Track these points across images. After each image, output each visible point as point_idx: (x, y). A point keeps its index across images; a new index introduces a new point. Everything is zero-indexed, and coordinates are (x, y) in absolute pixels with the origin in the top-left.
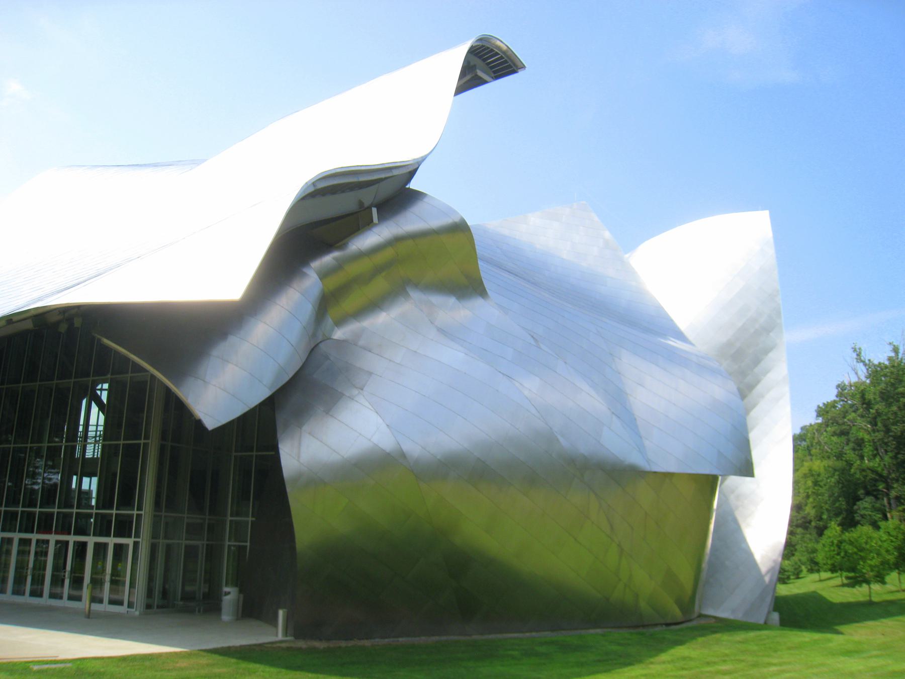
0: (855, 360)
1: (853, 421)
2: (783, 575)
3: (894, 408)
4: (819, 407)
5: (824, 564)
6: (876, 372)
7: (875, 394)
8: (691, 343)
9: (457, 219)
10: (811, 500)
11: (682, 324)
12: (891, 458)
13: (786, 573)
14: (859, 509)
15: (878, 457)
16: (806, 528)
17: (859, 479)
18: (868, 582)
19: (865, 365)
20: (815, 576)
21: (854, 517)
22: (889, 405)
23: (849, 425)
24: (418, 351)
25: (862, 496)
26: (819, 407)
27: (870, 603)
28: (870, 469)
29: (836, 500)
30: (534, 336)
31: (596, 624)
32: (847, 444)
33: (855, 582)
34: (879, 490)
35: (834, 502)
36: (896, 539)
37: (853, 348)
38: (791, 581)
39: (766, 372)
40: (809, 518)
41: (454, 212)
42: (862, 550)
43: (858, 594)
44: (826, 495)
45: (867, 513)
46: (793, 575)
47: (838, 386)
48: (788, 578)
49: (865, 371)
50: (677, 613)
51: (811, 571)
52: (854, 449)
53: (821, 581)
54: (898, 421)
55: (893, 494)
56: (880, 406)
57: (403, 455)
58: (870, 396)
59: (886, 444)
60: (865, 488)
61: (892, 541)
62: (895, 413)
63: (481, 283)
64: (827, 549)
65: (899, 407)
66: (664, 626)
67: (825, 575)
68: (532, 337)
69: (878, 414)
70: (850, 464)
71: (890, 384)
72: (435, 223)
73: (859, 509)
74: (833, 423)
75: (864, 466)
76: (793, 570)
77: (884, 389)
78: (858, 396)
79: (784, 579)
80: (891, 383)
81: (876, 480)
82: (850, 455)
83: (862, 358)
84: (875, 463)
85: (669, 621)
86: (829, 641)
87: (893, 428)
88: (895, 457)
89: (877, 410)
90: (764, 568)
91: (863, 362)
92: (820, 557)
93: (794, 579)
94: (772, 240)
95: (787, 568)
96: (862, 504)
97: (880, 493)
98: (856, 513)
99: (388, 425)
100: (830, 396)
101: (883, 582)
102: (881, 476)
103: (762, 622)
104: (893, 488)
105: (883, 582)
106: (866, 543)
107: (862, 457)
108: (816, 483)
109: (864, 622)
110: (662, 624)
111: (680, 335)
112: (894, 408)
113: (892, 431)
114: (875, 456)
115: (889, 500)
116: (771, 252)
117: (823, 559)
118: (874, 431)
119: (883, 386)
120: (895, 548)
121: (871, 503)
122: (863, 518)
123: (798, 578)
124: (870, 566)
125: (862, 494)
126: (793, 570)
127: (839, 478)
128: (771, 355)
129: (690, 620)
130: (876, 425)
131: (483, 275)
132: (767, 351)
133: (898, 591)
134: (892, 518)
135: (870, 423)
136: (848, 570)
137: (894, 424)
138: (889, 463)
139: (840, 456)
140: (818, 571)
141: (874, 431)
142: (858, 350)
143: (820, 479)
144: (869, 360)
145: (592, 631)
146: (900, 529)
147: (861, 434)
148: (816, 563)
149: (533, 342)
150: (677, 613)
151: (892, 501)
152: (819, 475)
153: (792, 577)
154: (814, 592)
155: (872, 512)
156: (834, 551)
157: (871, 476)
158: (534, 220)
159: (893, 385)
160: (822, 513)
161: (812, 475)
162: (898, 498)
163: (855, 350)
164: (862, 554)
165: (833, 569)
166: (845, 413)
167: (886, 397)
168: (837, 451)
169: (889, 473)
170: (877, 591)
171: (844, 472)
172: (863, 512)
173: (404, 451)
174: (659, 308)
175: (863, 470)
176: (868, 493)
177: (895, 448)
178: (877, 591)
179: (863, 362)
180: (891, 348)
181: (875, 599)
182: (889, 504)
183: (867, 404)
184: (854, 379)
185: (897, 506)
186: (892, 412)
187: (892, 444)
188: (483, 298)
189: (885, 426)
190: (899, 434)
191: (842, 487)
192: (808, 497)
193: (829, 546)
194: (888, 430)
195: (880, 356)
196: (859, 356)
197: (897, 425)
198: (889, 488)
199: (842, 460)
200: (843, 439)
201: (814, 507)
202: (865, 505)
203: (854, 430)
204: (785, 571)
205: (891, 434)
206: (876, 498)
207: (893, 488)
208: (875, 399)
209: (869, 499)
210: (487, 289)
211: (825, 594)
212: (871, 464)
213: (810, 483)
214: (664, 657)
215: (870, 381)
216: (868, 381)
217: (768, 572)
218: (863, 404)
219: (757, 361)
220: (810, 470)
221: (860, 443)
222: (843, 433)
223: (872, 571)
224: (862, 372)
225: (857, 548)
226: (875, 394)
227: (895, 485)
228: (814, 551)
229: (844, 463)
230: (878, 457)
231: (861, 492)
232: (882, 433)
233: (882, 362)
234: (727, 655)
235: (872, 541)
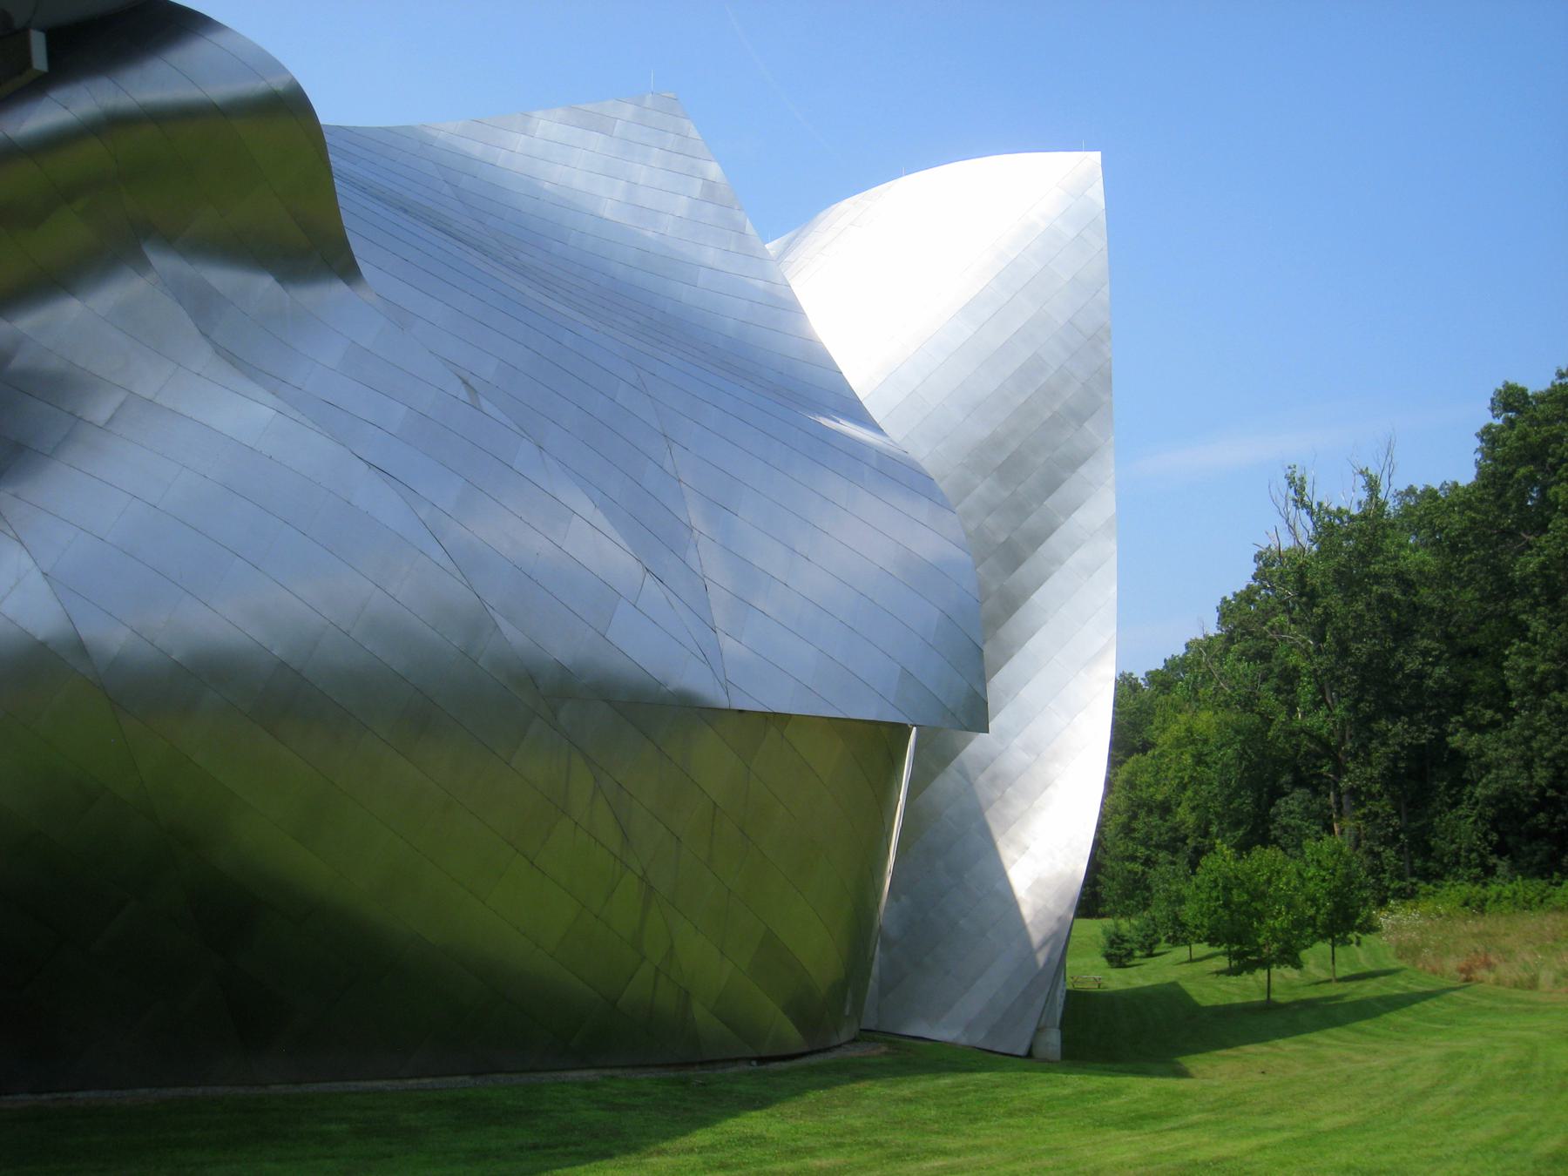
0: (1291, 503)
1: (1281, 629)
2: (1119, 949)
3: (1360, 606)
4: (1224, 600)
5: (1197, 927)
6: (1329, 527)
7: (1324, 574)
8: (877, 428)
9: (277, 84)
10: (1189, 793)
11: (861, 377)
12: (1347, 709)
13: (1127, 946)
14: (1279, 814)
15: (1324, 707)
16: (1175, 851)
17: (1283, 750)
18: (1265, 964)
19: (1311, 513)
20: (1182, 952)
21: (1269, 830)
22: (1350, 599)
23: (1272, 640)
24: (158, 400)
25: (1287, 788)
26: (1224, 600)
27: (1269, 1007)
28: (1306, 733)
29: (1235, 794)
30: (470, 382)
31: (1424, 999)
32: (1264, 680)
33: (1244, 962)
34: (1320, 776)
35: (1229, 799)
36: (1332, 874)
37: (1289, 478)
38: (1136, 961)
39: (1069, 510)
40: (1183, 831)
41: (280, 68)
42: (1261, 896)
43: (1248, 988)
44: (1216, 783)
45: (1293, 822)
46: (1141, 949)
47: (1258, 557)
48: (1130, 954)
49: (1310, 525)
50: (792, 1036)
51: (1175, 941)
52: (1278, 690)
53: (1191, 961)
54: (1364, 634)
55: (1345, 783)
56: (1334, 601)
57: (80, 648)
58: (1315, 580)
59: (1339, 679)
60: (1296, 770)
61: (1324, 880)
62: (1359, 617)
63: (345, 245)
64: (1203, 896)
65: (1368, 604)
66: (754, 1063)
67: (1202, 949)
68: (465, 382)
69: (1328, 617)
70: (1267, 721)
71: (1356, 554)
72: (219, 90)
73: (1279, 814)
74: (1243, 635)
75: (1295, 725)
76: (1141, 939)
77: (1344, 566)
78: (1291, 578)
79: (1121, 957)
80: (1359, 552)
81: (1318, 757)
82: (1268, 699)
83: (1306, 498)
84: (1317, 721)
85: (764, 1053)
86: (1117, 1092)
87: (1354, 646)
88: (1353, 708)
89: (1325, 608)
90: (1036, 937)
91: (1309, 508)
92: (1188, 912)
93: (1141, 957)
94: (1103, 219)
95: (1128, 935)
96: (1287, 803)
97: (1325, 780)
98: (1274, 822)
99: (45, 574)
100: (1240, 577)
101: (1298, 965)
102: (1326, 745)
103: (1022, 1051)
104: (1346, 771)
105: (1298, 965)
106: (1269, 882)
107: (1292, 711)
108: (1199, 759)
109: (1241, 1047)
110: (749, 1060)
111: (854, 410)
112: (1360, 606)
113: (1352, 655)
114: (1317, 705)
115: (1339, 795)
116: (1099, 243)
117: (1194, 917)
118: (1319, 651)
119: (1342, 558)
120: (1329, 893)
121: (1304, 801)
122: (1286, 832)
123: (1151, 955)
124: (1273, 930)
125: (1287, 783)
126: (1141, 939)
127: (1243, 749)
128: (1083, 470)
129: (828, 1050)
130: (1323, 640)
131: (347, 221)
132: (1074, 462)
133: (1329, 981)
134: (1342, 832)
135: (1313, 636)
136: (1230, 941)
137: (1357, 638)
138: (1343, 720)
139: (1248, 703)
140: (1186, 942)
141: (1319, 651)
142: (1298, 482)
143: (1206, 750)
144: (1320, 505)
145: (573, 1075)
146: (1341, 853)
147: (1293, 660)
148: (1183, 925)
149: (463, 394)
150: (792, 1036)
151: (1345, 799)
152: (1206, 742)
153: (1138, 953)
154: (1174, 984)
155: (1302, 820)
156: (1217, 899)
157: (1307, 744)
158: (548, 126)
159: (1362, 556)
160: (1209, 823)
161: (1193, 742)
162: (1354, 792)
163: (1291, 482)
164: (1259, 906)
165: (1212, 940)
166: (1269, 613)
167: (1346, 581)
168: (1243, 691)
169: (1342, 741)
170: (1285, 982)
171: (1254, 737)
172: (1285, 821)
173: (83, 639)
174: (824, 349)
175: (1292, 734)
176: (1299, 782)
177: (1355, 689)
178: (1285, 982)
179: (1309, 508)
180: (1361, 481)
181: (1280, 997)
182: (1339, 803)
183: (1309, 596)
184: (1287, 543)
185: (1354, 808)
186: (1354, 614)
187: (1350, 683)
188: (348, 283)
189: (1340, 642)
190: (1364, 659)
191: (1246, 769)
192: (1183, 787)
193: (1208, 890)
194: (1344, 652)
195: (1347, 497)
196: (1300, 494)
197: (1361, 642)
198: (1339, 770)
199: (1252, 711)
200: (1261, 667)
201: (1193, 809)
202: (1292, 804)
203: (1281, 651)
204: (1124, 941)
205: (1349, 660)
206: (1316, 792)
207: (1346, 771)
208: (1323, 584)
209: (1300, 793)
210: (359, 262)
211: (1192, 989)
212: (1308, 722)
213: (1187, 759)
214: (702, 1137)
215: (1319, 548)
216: (1314, 548)
217: (1044, 943)
218: (1301, 595)
219: (1052, 485)
220: (1189, 730)
221: (1290, 677)
222: (1263, 656)
223: (1276, 939)
224: (1305, 524)
225: (1248, 893)
226: (1324, 574)
227: (1351, 766)
228: (1181, 900)
229: (1257, 719)
230: (1324, 707)
231: (1286, 778)
232: (1333, 658)
233: (1344, 507)
234: (854, 1131)
235: (1279, 879)
